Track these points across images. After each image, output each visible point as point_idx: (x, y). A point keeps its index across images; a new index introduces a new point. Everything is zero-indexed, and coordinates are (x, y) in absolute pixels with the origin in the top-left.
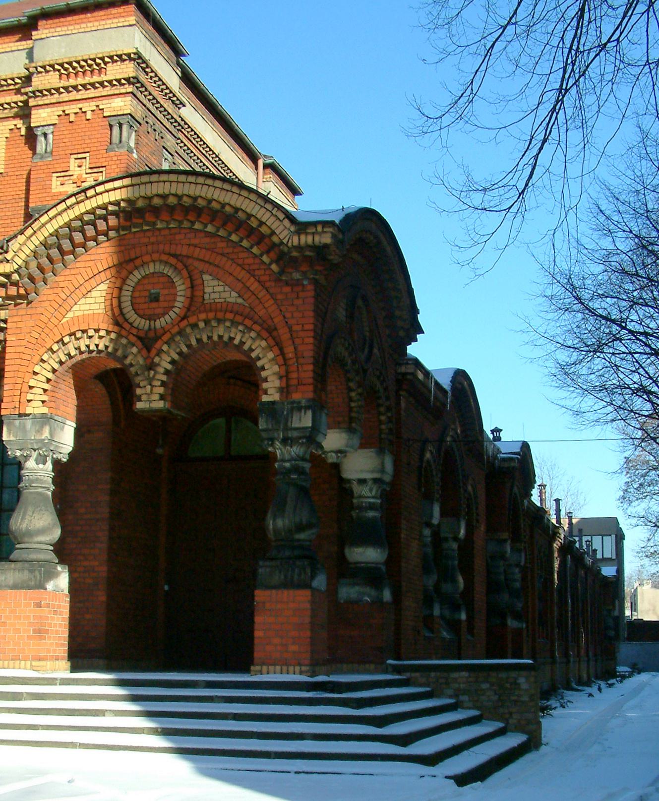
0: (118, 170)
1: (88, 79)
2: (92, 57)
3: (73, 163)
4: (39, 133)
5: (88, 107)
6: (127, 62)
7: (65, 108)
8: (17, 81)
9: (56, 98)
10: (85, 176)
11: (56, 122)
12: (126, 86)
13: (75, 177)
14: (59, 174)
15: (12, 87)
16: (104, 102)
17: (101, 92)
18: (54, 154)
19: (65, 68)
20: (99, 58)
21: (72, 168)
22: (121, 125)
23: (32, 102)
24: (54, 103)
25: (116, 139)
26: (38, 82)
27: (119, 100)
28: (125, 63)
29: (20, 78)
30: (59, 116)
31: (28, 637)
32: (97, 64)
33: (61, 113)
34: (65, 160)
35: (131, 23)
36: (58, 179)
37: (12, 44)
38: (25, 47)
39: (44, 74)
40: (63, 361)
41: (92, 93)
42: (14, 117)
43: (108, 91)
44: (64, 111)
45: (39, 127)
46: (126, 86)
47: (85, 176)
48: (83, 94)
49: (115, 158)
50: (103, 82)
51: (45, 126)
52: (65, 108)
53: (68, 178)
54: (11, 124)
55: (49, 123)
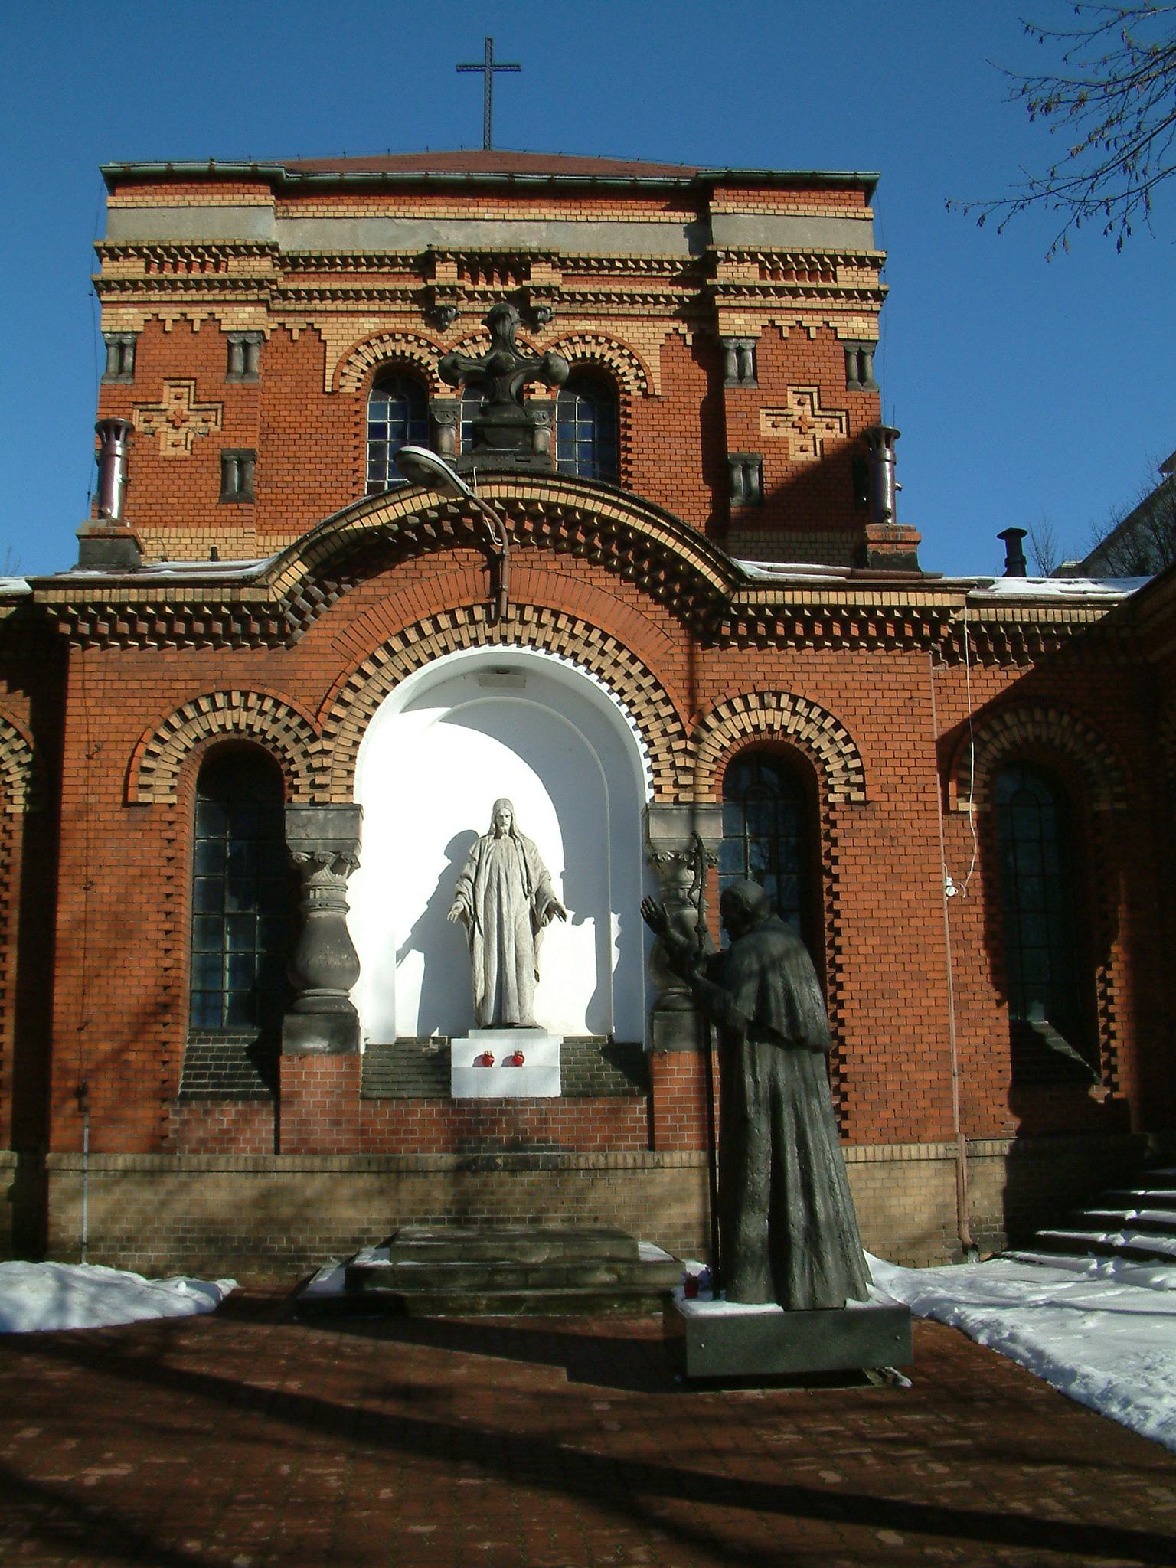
0: (867, 418)
1: (807, 284)
2: (817, 252)
3: (168, 393)
4: (731, 347)
5: (812, 322)
6: (748, 264)
7: (774, 317)
8: (679, 266)
9: (758, 300)
10: (186, 412)
11: (759, 334)
12: (871, 302)
13: (170, 413)
14: (770, 411)
15: (666, 274)
16: (836, 318)
17: (829, 302)
18: (136, 375)
19: (773, 263)
20: (815, 256)
21: (165, 399)
22: (246, 346)
23: (719, 300)
24: (755, 308)
25: (238, 366)
26: (724, 274)
27: (860, 319)
28: (132, 259)
29: (681, 263)
30: (763, 327)
31: (317, 1115)
32: (821, 266)
33: (767, 323)
34: (780, 392)
35: (867, 216)
36: (768, 418)
37: (658, 213)
38: (683, 220)
39: (735, 263)
40: (653, 681)
41: (816, 302)
42: (672, 318)
43: (841, 303)
44: (770, 321)
45: (731, 337)
46: (871, 302)
47: (186, 412)
48: (810, 303)
49: (861, 401)
50: (125, 281)
51: (742, 337)
52: (774, 317)
53: (784, 418)
54: (669, 326)
55: (749, 334)
